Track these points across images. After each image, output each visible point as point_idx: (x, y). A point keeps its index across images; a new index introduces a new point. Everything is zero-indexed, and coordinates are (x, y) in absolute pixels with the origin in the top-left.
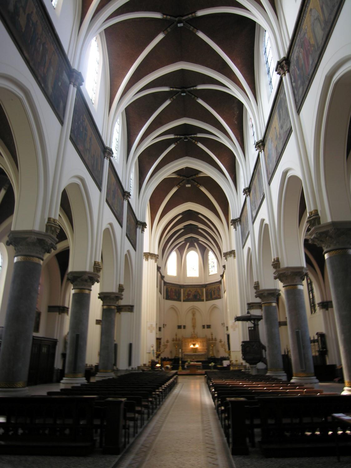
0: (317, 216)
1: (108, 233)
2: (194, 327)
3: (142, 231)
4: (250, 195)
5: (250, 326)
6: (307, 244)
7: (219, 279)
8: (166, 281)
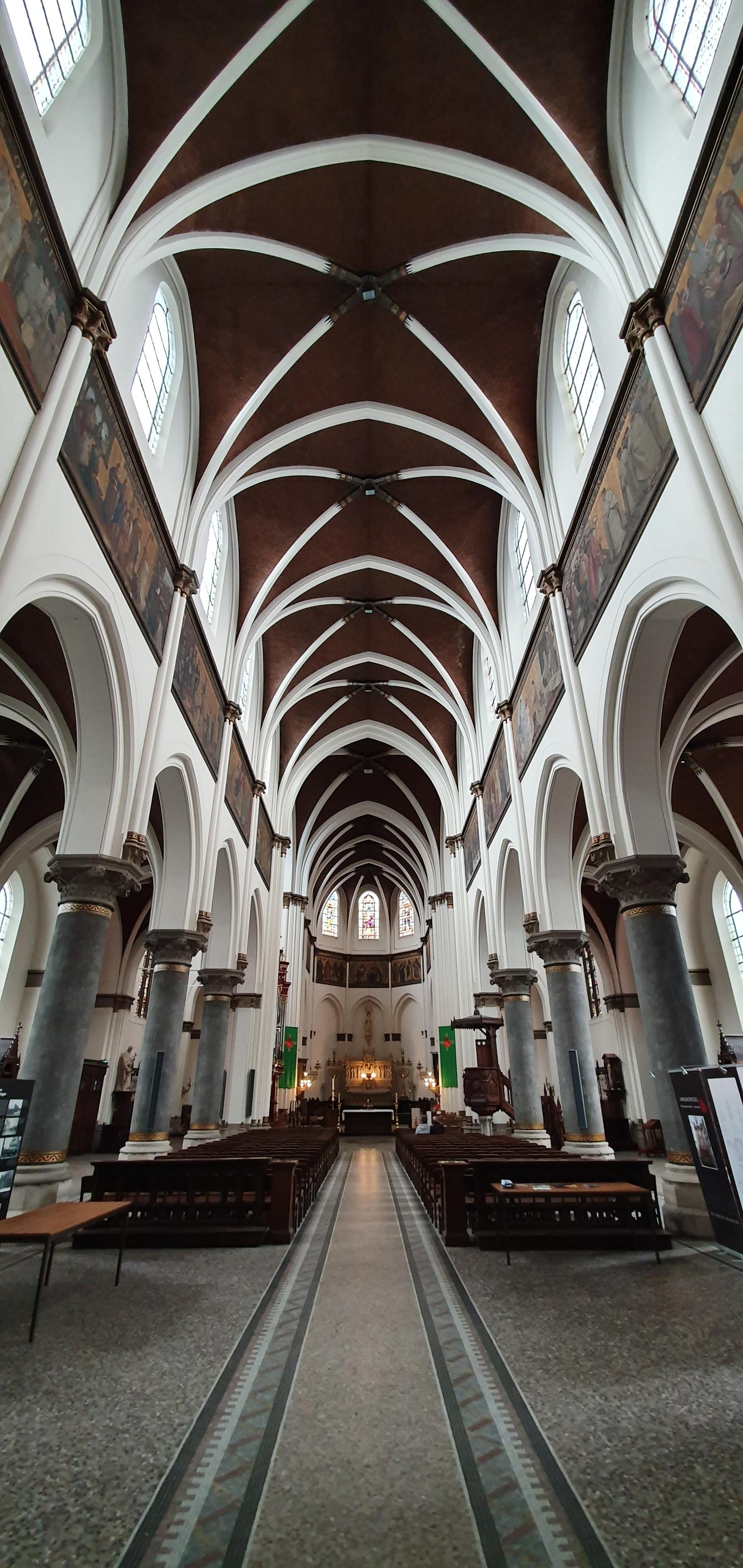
0: (610, 844)
1: (225, 859)
2: (369, 1037)
3: (282, 853)
4: (510, 718)
5: (479, 1039)
6: (587, 889)
7: (419, 944)
8: (317, 946)
